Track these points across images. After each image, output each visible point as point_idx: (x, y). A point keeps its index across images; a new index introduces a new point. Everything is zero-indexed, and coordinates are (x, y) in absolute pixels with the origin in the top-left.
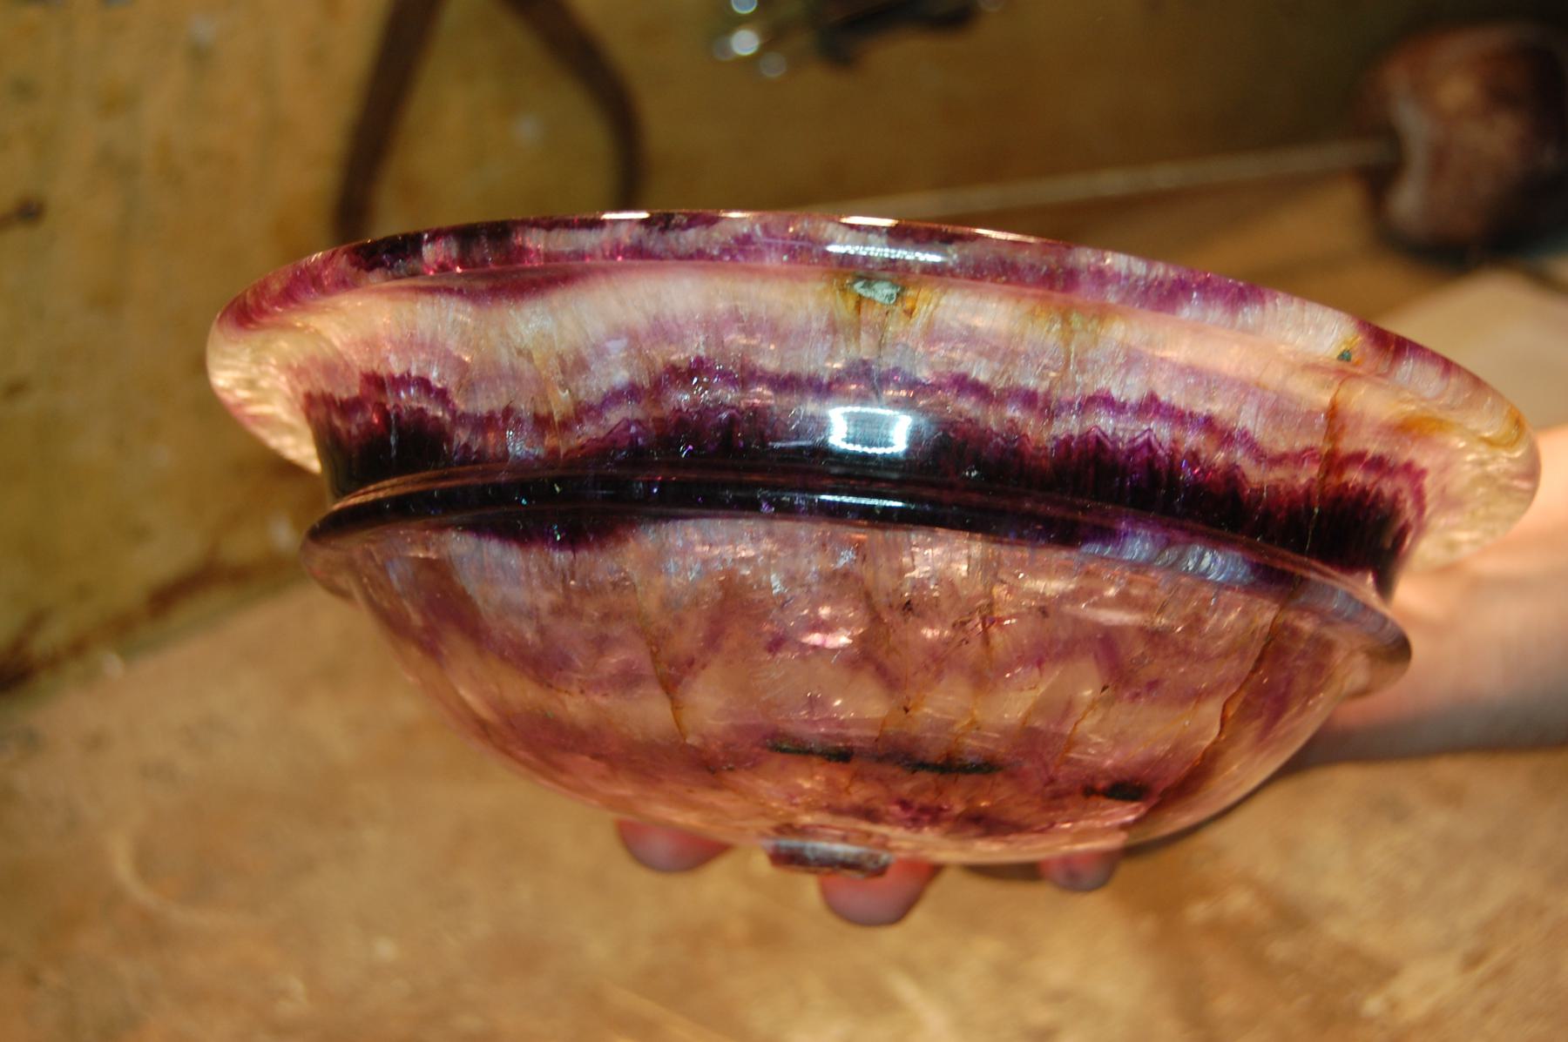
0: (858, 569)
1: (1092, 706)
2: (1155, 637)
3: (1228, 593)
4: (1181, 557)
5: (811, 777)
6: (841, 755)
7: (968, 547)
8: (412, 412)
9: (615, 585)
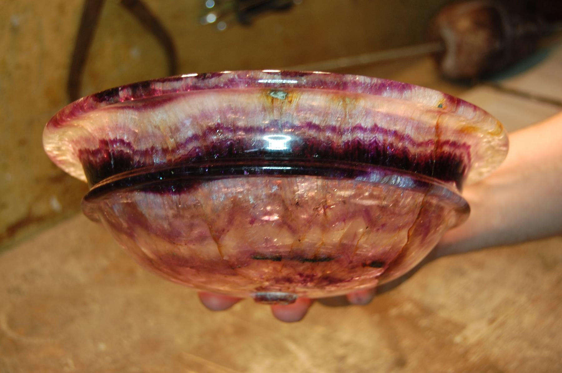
0: (279, 192)
1: (363, 234)
2: (383, 209)
3: (407, 191)
4: (390, 179)
5: (268, 267)
6: (278, 259)
7: (317, 181)
8: (119, 152)
9: (195, 205)
